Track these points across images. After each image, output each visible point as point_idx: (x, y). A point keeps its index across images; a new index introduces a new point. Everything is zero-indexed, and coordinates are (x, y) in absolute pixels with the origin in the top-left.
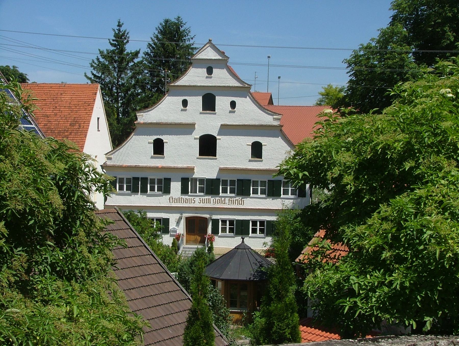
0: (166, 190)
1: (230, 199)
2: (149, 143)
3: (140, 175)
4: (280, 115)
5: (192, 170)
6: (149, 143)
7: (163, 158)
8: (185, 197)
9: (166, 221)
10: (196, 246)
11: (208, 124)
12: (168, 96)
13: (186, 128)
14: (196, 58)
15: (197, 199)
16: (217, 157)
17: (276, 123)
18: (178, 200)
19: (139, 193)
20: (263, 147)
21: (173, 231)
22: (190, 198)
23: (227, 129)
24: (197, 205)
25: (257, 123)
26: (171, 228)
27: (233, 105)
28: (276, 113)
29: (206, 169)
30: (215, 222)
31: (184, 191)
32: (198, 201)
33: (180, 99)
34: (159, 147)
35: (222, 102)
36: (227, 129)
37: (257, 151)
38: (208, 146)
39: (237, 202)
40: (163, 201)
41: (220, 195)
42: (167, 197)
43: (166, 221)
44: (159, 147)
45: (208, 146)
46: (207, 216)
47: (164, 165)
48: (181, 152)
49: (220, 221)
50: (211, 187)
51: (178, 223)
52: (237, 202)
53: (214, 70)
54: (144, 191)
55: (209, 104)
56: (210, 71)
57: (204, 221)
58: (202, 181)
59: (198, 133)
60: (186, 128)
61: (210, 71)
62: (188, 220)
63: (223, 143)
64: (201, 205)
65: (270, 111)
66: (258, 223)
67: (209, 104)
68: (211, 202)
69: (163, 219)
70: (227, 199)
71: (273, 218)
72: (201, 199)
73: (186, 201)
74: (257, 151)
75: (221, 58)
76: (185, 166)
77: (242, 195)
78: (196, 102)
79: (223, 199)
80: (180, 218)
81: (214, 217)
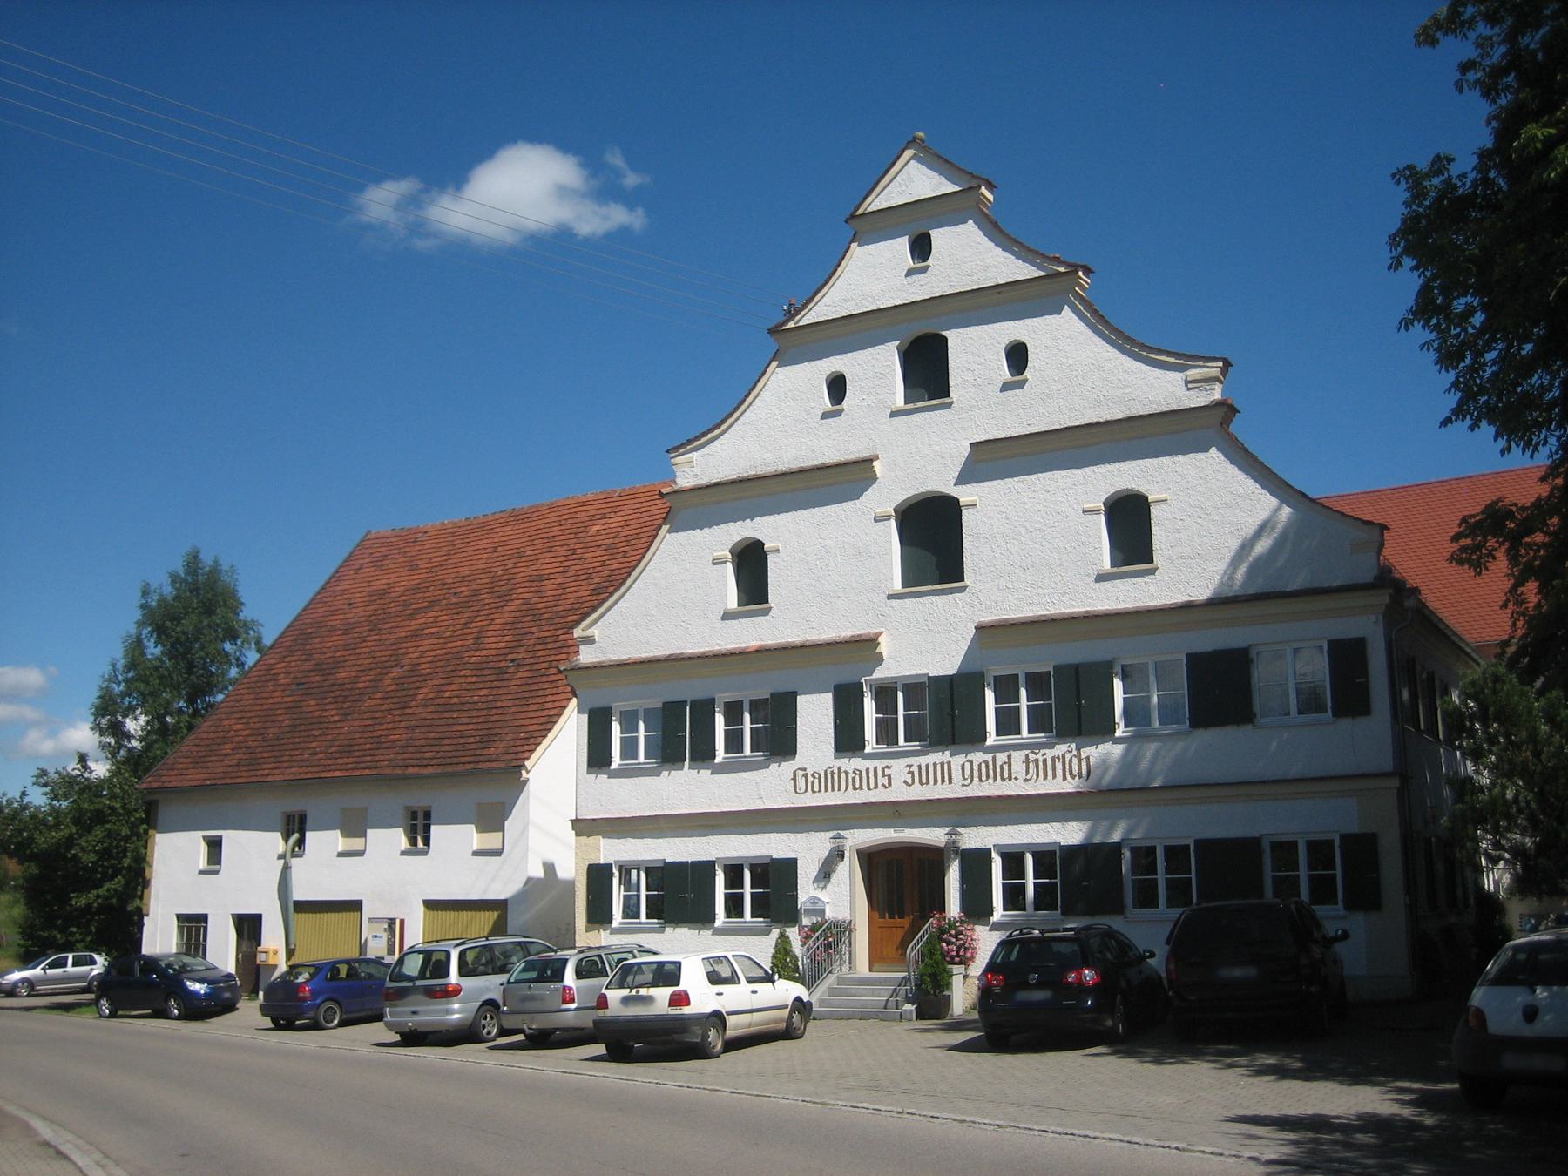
0: (778, 739)
1: (1032, 757)
2: (717, 562)
3: (688, 690)
4: (1215, 359)
5: (865, 647)
6: (717, 562)
7: (766, 612)
8: (852, 764)
9: (787, 869)
10: (1416, 1086)
11: (921, 453)
12: (669, 531)
13: (845, 479)
14: (873, 208)
15: (898, 767)
16: (967, 581)
17: (1199, 399)
18: (827, 780)
19: (687, 763)
20: (1154, 511)
21: (809, 912)
22: (871, 764)
23: (993, 458)
24: (900, 792)
25: (1118, 413)
26: (802, 897)
27: (1017, 356)
28: (1195, 357)
29: (925, 640)
30: (976, 863)
31: (848, 739)
32: (904, 774)
33: (818, 371)
34: (751, 566)
35: (973, 352)
36: (993, 458)
37: (1130, 525)
38: (933, 539)
39: (1059, 766)
40: (770, 786)
41: (989, 742)
42: (787, 767)
43: (787, 869)
44: (751, 566)
45: (933, 539)
46: (934, 836)
47: (771, 640)
48: (837, 575)
49: (995, 855)
50: (945, 713)
51: (825, 874)
52: (1059, 766)
53: (939, 236)
54: (703, 755)
55: (927, 372)
56: (921, 248)
57: (930, 862)
58: (916, 689)
59: (893, 488)
60: (845, 479)
61: (921, 248)
62: (875, 863)
63: (989, 513)
64: (918, 793)
65: (1169, 354)
66: (1029, 860)
67: (927, 372)
68: (957, 774)
69: (1062, 848)
70: (1018, 757)
71: (1070, 833)
72: (915, 769)
73: (858, 781)
74: (1130, 525)
75: (957, 188)
76: (846, 633)
77: (1080, 734)
78: (878, 370)
79: (1001, 757)
80: (838, 854)
81: (974, 837)
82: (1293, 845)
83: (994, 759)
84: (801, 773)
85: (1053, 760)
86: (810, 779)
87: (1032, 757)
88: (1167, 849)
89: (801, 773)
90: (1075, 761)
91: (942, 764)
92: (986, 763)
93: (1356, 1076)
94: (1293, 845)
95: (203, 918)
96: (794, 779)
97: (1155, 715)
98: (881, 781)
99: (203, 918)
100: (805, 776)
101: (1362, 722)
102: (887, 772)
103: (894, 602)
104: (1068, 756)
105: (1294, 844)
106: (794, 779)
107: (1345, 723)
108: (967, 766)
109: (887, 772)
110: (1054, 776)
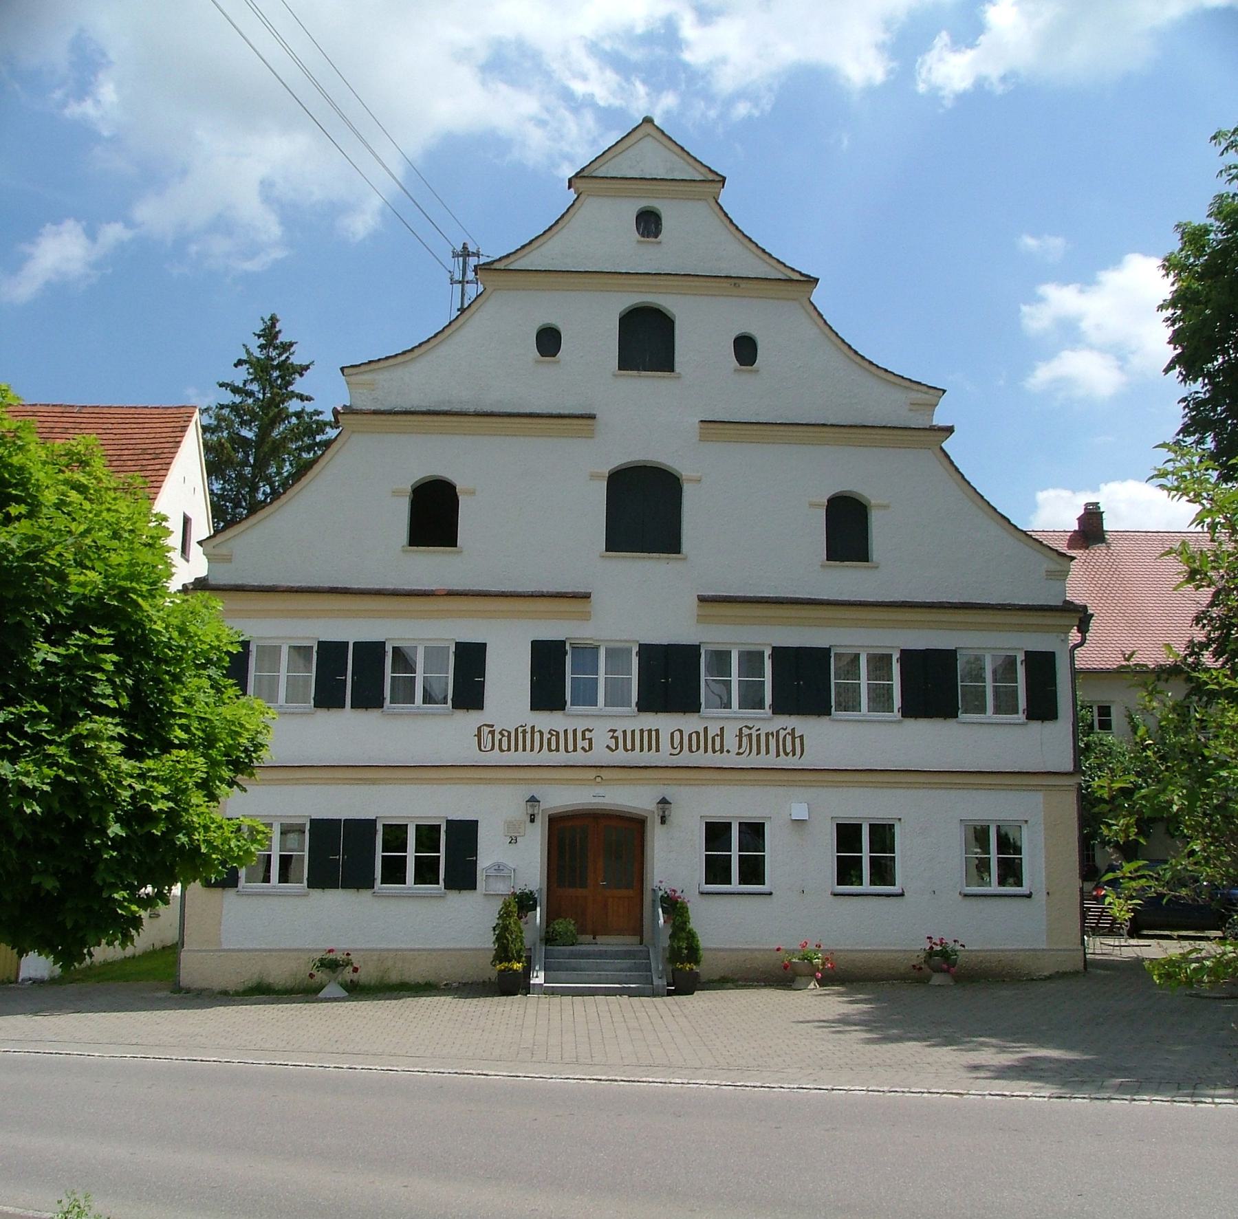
18: (520, 737)
29: (642, 603)
38: (644, 510)
39: (772, 742)
45: (644, 510)
52: (772, 742)
72: (619, 734)
82: (403, 828)
83: (706, 729)
84: (487, 729)
85: (767, 735)
86: (497, 737)
87: (746, 731)
88: (873, 827)
89: (487, 729)
90: (789, 738)
91: (650, 731)
92: (698, 733)
93: (1071, 1048)
94: (403, 828)
95: (473, 825)
96: (479, 735)
97: (989, 675)
98: (580, 743)
99: (473, 825)
100: (492, 733)
101: (1049, 725)
102: (588, 735)
103: (582, 589)
104: (782, 733)
105: (858, 827)
106: (479, 735)
107: (1036, 726)
108: (677, 734)
109: (588, 735)
110: (768, 752)
